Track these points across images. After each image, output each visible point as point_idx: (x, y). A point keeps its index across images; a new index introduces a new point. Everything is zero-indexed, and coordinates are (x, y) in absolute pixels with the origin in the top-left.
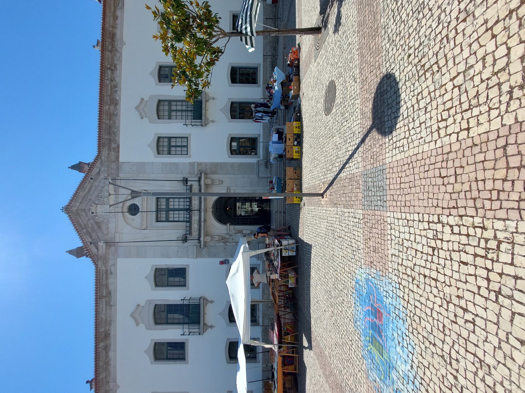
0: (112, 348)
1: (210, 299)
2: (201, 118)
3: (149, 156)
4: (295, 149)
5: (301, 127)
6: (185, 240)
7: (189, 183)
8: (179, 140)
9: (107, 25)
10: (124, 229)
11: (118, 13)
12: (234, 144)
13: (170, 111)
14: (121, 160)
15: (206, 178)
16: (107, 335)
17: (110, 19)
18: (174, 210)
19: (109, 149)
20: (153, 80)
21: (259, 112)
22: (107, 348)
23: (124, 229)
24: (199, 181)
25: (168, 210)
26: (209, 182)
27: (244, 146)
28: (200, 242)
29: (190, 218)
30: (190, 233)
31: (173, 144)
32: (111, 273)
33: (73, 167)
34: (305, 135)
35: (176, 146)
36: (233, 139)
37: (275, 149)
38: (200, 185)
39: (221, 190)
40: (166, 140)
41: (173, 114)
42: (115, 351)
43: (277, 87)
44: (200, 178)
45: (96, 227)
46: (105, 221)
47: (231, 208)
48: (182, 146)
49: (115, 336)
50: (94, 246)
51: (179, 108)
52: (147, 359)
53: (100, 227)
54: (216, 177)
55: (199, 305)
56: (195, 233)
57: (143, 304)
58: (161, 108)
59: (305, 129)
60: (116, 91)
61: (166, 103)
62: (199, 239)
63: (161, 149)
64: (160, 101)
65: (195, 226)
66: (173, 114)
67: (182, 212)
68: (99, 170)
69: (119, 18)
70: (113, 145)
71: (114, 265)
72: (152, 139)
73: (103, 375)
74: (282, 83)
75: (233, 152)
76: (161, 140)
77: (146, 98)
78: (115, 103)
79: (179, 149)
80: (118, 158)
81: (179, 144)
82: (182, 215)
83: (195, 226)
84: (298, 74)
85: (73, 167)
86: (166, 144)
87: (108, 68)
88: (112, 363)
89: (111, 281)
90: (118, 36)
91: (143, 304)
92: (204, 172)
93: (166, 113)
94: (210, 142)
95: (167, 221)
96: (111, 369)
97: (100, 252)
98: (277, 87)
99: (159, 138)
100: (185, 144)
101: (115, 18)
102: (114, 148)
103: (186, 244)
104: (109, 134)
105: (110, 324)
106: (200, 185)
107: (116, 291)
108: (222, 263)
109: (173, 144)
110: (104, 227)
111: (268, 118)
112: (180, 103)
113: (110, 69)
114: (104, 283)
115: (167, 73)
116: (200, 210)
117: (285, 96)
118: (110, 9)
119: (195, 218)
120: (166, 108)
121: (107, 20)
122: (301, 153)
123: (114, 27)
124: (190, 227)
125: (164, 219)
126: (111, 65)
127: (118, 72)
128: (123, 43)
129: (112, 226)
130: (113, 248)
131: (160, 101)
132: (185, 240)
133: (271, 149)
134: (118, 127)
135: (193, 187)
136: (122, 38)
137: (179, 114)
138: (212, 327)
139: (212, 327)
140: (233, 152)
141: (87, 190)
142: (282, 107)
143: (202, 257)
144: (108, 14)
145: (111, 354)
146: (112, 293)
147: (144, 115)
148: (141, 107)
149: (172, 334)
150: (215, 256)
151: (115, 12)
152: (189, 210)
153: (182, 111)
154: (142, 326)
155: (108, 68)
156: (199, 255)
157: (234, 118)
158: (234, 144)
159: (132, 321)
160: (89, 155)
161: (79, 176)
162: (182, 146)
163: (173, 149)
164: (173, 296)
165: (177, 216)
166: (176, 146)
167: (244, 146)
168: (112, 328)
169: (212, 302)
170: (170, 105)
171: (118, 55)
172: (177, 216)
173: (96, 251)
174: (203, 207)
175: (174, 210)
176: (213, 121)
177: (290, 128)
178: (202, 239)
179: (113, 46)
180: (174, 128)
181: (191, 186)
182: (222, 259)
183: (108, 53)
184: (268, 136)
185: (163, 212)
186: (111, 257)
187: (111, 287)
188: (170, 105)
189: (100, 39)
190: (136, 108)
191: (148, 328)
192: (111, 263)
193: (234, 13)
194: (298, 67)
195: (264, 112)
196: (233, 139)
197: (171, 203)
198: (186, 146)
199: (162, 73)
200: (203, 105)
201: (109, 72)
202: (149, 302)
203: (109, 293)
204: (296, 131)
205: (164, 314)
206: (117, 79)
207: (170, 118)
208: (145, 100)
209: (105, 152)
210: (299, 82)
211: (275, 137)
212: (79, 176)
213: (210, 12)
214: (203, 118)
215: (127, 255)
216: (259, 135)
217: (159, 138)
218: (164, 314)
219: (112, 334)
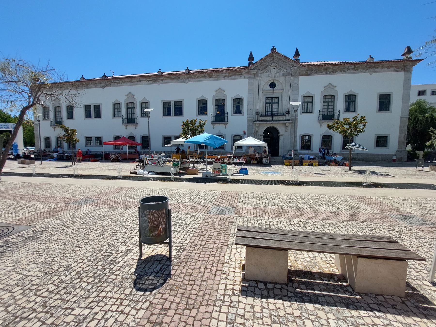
0: (205, 79)
1: (227, 126)
2: (323, 119)
3: (302, 92)
4: (307, 164)
5: (316, 166)
6: (258, 113)
7: (287, 115)
8: (311, 108)
9: (383, 64)
10: (264, 82)
11: (392, 69)
12: (307, 137)
13: (328, 102)
14: (301, 77)
15: (289, 123)
16: (210, 77)
17: (387, 65)
18: (272, 106)
19: (307, 71)
20: (347, 91)
21: (325, 151)
22: (205, 77)
23: (264, 82)
24: (288, 120)
25: (272, 103)
26: (287, 125)
27: (306, 143)
28: (256, 121)
29: (268, 116)
30: (261, 116)
31: (309, 104)
32: (241, 76)
33: (297, 51)
34: (312, 167)
35: (307, 106)
36: (310, 137)
37: (306, 157)
38: (286, 120)
39: (281, 129)
40: (311, 100)
41: (326, 104)
42: (203, 81)
43: (334, 157)
44: (289, 120)
45: (264, 66)
46: (267, 71)
47: (268, 135)
48: (307, 109)
49: (210, 80)
50: (253, 67)
51: (330, 107)
52: (199, 97)
53: (264, 68)
54: (289, 128)
55: (224, 121)
56: (260, 118)
57: (225, 93)
58: (330, 97)
59: (315, 167)
60: (341, 71)
61: (333, 100)
62: (258, 121)
63: (306, 98)
64: (334, 96)
65: (264, 118)
66: (326, 104)
67: (270, 110)
68: (295, 66)
69: (389, 70)
70: (309, 72)
71: (245, 78)
72: (312, 93)
73: (192, 76)
74: (336, 160)
75: (303, 137)
76: (311, 98)
77: (336, 89)
78: (334, 72)
79: (306, 108)
80: (302, 75)
81: (308, 108)
82: (269, 111)
83: (264, 118)
84: (339, 166)
85: (297, 51)
86: (309, 100)
87: (356, 66)
88: (197, 80)
89: (237, 76)
90: (376, 70)
91: (225, 93)
92: (293, 122)
93: (327, 100)
94: (310, 125)
95: (266, 103)
96: (195, 79)
97: (252, 71)
98: (334, 157)
99: (312, 97)
100: (308, 111)
101: (388, 68)
102: (307, 73)
103: (254, 113)
104: (316, 70)
105: (215, 77)
106: (286, 120)
107: (232, 79)
108: (244, 132)
109: (309, 104)
110: (264, 71)
111: (321, 155)
112: (332, 107)
113: (355, 67)
114: (236, 74)
115: (352, 99)
116: (272, 121)
117: (331, 161)
118: (394, 64)
119: (268, 118)
120: (330, 100)
121: (387, 63)
122: (305, 165)
123: (382, 67)
124: (264, 116)
125: (267, 101)
126: (357, 67)
127: (353, 71)
128: (371, 73)
129: (264, 75)
130: (253, 76)
131: (334, 96)
132: (258, 113)
133: (305, 155)
134: (319, 74)
135: (284, 117)
136: (375, 72)
137: (326, 107)
138: (214, 127)
139: (214, 127)
140: (303, 137)
141: (284, 61)
142: (326, 161)
143: (247, 122)
144: (390, 64)
145: (202, 79)
146: (231, 78)
147: (326, 88)
148: (331, 86)
149: (211, 108)
150: (248, 128)
151: (393, 67)
152: (272, 115)
153: (328, 109)
154: (214, 93)
155: (356, 66)
156: (248, 120)
157: (322, 138)
158: (307, 137)
159: (217, 88)
160: (304, 60)
161: (291, 55)
162: (307, 109)
163: (306, 104)
164: (229, 108)
165: (269, 107)
166: (307, 106)
167: (306, 143)
168: (214, 79)
169: (225, 127)
170: (331, 102)
171: (364, 71)
172: (269, 107)
173: (252, 68)
174: (274, 122)
175: (272, 106)
176: (321, 126)
177: (316, 162)
178: (258, 122)
179: (369, 68)
180: (318, 105)
181: (285, 116)
182: (246, 131)
183: (365, 65)
184: (312, 154)
185: (272, 101)
186: (249, 76)
187: (233, 77)
188: (331, 102)
189: (375, 60)
190: (330, 84)
191: (214, 96)
192: (246, 76)
193: (388, 138)
194: (342, 166)
195: (324, 153)
196: (310, 137)
197: (275, 104)
198: (307, 112)
199: (352, 97)
200: (330, 121)
201: (353, 67)
202: (226, 96)
203: (231, 76)
204: (314, 164)
205: (220, 105)
206: (348, 71)
207: (324, 102)
208: (335, 88)
209: (305, 69)
210: (336, 166)
211: (311, 157)
212: (291, 55)
213: (361, 132)
214: (323, 121)
215: (249, 84)
216: (312, 151)
217: (312, 97)
218: (220, 105)
219: (211, 79)
